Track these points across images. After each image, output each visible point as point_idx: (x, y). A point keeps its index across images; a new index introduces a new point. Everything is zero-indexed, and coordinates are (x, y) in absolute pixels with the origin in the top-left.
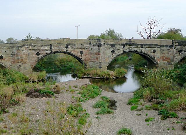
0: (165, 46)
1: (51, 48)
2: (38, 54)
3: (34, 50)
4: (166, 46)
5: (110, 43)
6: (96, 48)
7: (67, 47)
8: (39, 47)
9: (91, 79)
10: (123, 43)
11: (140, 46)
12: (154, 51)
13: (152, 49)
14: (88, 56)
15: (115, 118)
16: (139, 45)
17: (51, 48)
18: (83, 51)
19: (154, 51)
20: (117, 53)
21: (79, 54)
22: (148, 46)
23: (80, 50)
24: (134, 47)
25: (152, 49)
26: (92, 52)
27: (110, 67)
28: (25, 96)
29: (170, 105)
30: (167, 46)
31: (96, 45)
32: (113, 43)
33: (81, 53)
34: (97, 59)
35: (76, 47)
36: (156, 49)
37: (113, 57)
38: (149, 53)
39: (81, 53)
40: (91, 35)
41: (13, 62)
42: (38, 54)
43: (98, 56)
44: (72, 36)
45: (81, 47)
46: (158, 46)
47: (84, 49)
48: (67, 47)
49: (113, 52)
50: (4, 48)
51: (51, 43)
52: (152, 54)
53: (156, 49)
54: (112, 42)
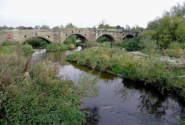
2: (67, 35)
3: (65, 33)
6: (93, 33)
7: (79, 32)
11: (109, 32)
12: (114, 34)
13: (113, 33)
15: (98, 62)
16: (109, 31)
19: (114, 34)
20: (100, 35)
22: (112, 32)
23: (85, 33)
25: (113, 33)
26: (91, 34)
27: (65, 43)
33: (86, 35)
34: (94, 38)
35: (83, 32)
37: (98, 37)
38: (84, 36)
39: (86, 35)
40: (48, 25)
41: (56, 39)
42: (67, 35)
43: (94, 36)
45: (86, 32)
48: (79, 32)
49: (99, 34)
50: (50, 31)
52: (113, 36)
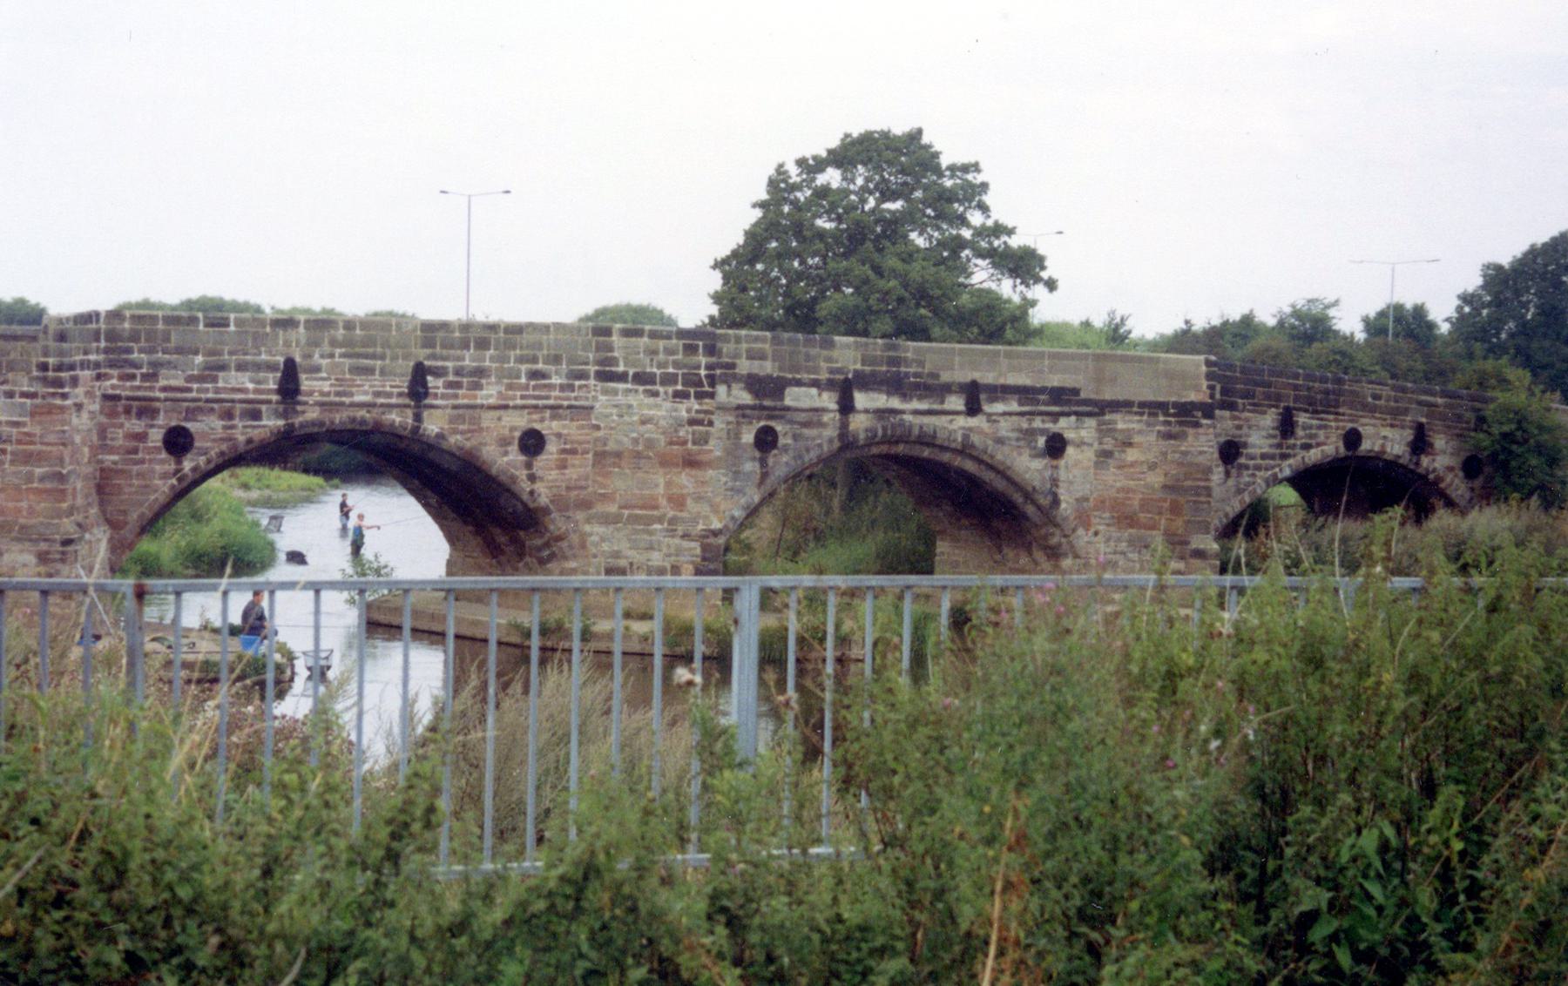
0: (1142, 405)
1: (289, 387)
4: (1153, 408)
5: (744, 366)
7: (418, 390)
8: (190, 379)
9: (510, 650)
10: (839, 371)
11: (956, 402)
12: (1056, 446)
14: (579, 468)
17: (289, 387)
18: (549, 427)
21: (515, 456)
23: (519, 422)
24: (916, 405)
28: (1419, 534)
29: (1509, 659)
30: (1162, 407)
31: (668, 380)
32: (768, 368)
36: (1065, 426)
39: (532, 443)
44: (228, 296)
46: (1086, 402)
47: (552, 407)
48: (418, 390)
51: (294, 345)
52: (1029, 467)
53: (1065, 426)
54: (763, 357)
